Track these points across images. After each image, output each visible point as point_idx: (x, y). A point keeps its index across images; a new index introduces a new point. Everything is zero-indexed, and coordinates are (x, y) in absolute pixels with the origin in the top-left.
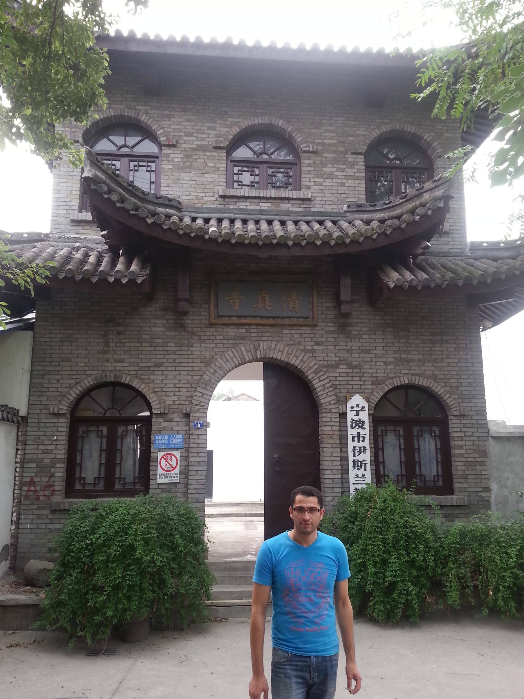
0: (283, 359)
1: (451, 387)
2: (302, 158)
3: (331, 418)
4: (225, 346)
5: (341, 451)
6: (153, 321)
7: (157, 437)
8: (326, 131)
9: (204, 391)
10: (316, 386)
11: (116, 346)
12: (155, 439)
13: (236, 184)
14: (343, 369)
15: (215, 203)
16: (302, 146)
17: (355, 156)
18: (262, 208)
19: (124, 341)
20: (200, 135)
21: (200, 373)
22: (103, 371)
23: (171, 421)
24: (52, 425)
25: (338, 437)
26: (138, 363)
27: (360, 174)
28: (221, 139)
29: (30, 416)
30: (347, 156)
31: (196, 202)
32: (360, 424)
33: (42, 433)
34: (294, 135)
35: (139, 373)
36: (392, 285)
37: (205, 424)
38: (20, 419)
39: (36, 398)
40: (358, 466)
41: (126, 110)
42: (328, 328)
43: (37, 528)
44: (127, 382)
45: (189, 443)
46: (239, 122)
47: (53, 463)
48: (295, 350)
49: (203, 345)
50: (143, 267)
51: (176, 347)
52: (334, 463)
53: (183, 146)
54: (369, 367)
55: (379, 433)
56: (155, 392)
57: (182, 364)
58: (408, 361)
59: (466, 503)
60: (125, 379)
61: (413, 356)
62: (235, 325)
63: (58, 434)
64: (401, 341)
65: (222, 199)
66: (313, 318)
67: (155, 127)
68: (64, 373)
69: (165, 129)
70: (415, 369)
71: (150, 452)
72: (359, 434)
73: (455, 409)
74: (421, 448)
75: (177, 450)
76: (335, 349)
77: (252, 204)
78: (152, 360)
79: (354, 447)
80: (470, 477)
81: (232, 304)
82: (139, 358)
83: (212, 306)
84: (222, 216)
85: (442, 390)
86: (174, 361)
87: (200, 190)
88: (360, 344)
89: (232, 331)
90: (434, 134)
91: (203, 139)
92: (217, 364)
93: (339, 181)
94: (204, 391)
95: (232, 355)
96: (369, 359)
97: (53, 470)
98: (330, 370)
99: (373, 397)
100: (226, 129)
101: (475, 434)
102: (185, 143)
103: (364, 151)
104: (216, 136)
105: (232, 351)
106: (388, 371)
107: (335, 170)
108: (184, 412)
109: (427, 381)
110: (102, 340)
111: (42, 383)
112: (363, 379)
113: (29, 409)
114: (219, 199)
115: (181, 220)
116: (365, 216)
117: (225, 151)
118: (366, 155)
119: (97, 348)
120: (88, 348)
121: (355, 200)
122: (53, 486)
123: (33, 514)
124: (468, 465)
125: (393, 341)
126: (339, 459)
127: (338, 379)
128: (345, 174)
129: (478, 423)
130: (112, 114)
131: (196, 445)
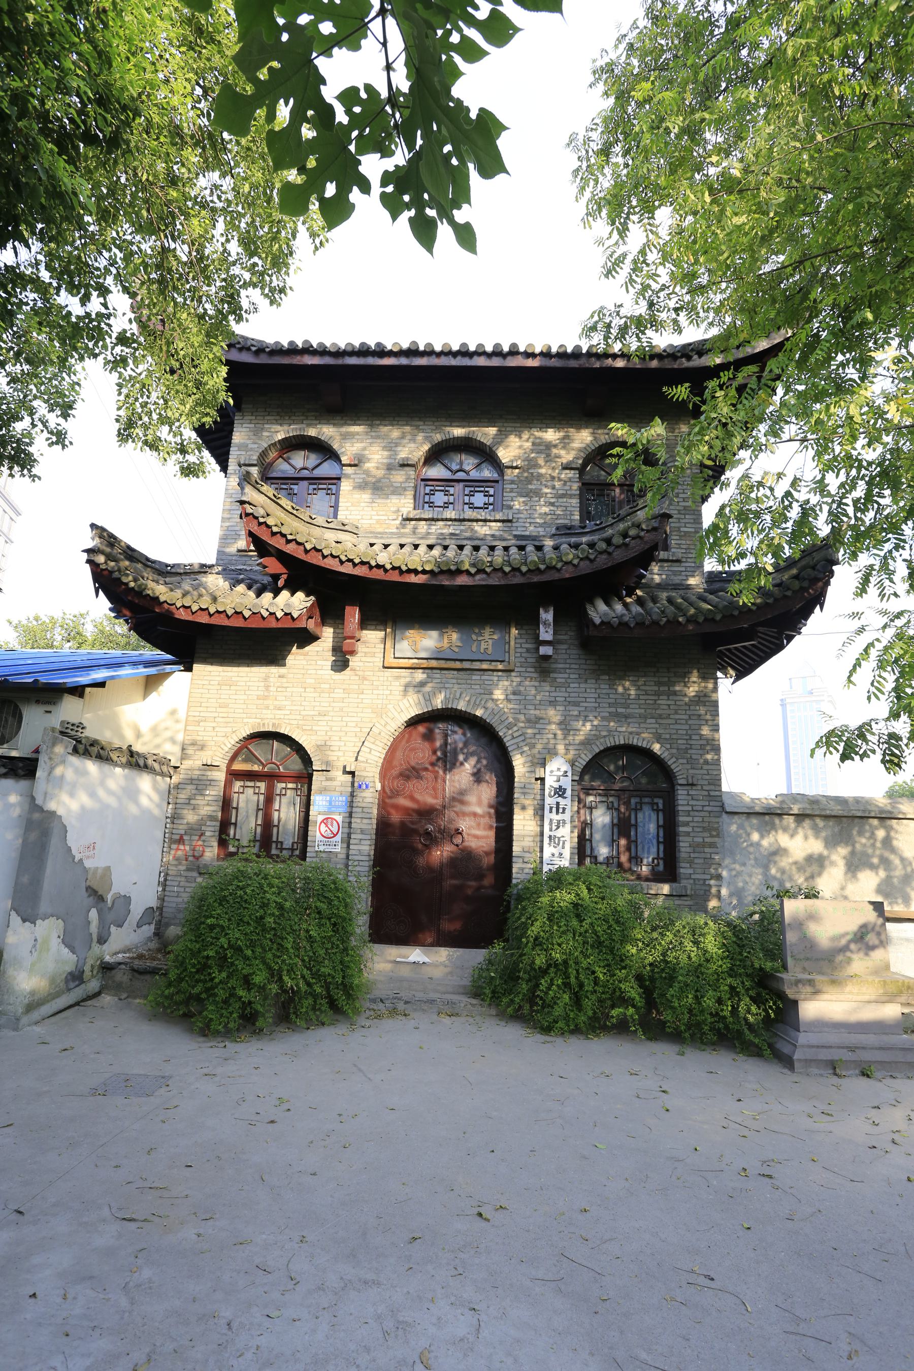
13: (426, 506)
36: (597, 621)
72: (558, 804)
74: (640, 824)
80: (696, 861)
86: (341, 710)
92: (390, 714)
101: (706, 808)
116: (573, 540)
118: (581, 470)
121: (566, 521)
124: (695, 847)
129: (709, 795)
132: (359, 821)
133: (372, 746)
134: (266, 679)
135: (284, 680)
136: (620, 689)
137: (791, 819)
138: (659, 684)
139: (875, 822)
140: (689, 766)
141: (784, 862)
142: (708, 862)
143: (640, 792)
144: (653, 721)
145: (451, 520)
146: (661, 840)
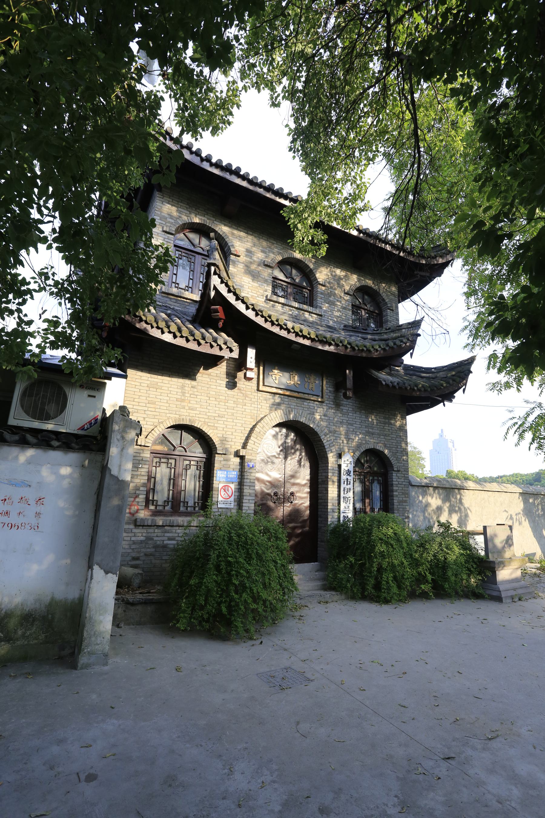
19: (196, 393)
22: (180, 415)
35: (207, 420)
68: (150, 413)
110: (180, 391)
119: (176, 396)
132: (248, 488)
133: (255, 440)
134: (183, 387)
135: (195, 390)
136: (370, 420)
137: (431, 489)
138: (385, 418)
139: (457, 491)
141: (430, 510)
142: (405, 510)
143: (373, 474)
145: (295, 308)
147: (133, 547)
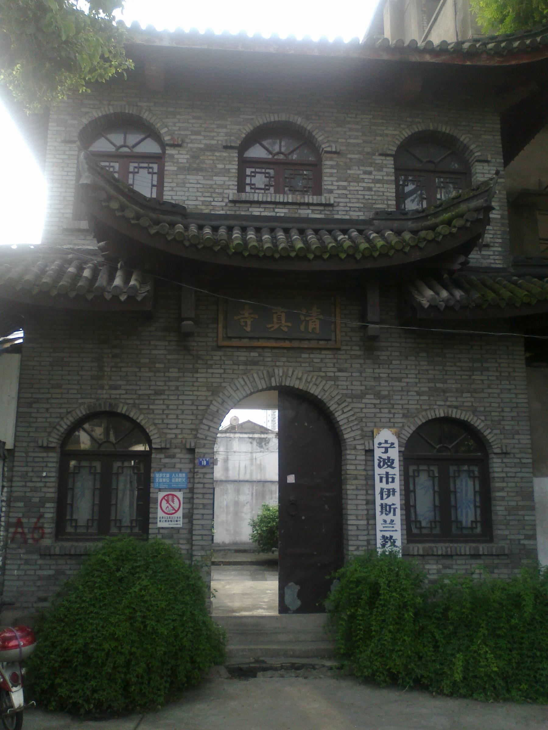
0: (301, 388)
1: (492, 421)
2: (324, 159)
3: (356, 455)
4: (235, 372)
5: (367, 494)
6: (152, 343)
7: (157, 475)
8: (350, 130)
9: (211, 424)
10: (338, 419)
11: (111, 371)
12: (154, 478)
14: (370, 399)
15: (225, 208)
16: (323, 146)
17: (383, 158)
18: (278, 215)
19: (121, 365)
20: (208, 134)
21: (206, 403)
22: (98, 399)
23: (173, 456)
24: (40, 460)
25: (363, 478)
26: (136, 390)
27: (389, 178)
28: (232, 138)
29: (16, 449)
30: (374, 157)
31: (203, 207)
32: (389, 462)
33: (30, 469)
34: (314, 133)
35: (137, 401)
37: (211, 461)
38: (6, 453)
39: (23, 429)
40: (386, 510)
41: (127, 107)
42: (353, 353)
43: (25, 575)
44: (123, 412)
45: (194, 483)
46: (253, 119)
47: (43, 501)
48: (315, 377)
49: (210, 371)
50: (143, 282)
51: (179, 372)
52: (360, 507)
53: (190, 145)
54: (399, 397)
55: (411, 473)
56: (155, 424)
57: (186, 393)
58: (445, 391)
59: (506, 552)
60: (122, 409)
61: (449, 386)
62: (246, 347)
63: (48, 469)
64: (437, 368)
65: (233, 205)
66: (336, 341)
67: (159, 125)
68: (54, 401)
69: (170, 128)
70: (452, 400)
71: (149, 492)
72: (387, 474)
73: (496, 446)
74: (458, 490)
75: (180, 490)
76: (361, 376)
77: (267, 210)
78: (152, 388)
79: (382, 490)
81: (243, 324)
82: (137, 385)
83: (220, 325)
84: (231, 223)
85: (482, 425)
86: (177, 388)
87: (207, 194)
88: (389, 371)
89: (242, 356)
90: (471, 136)
91: (212, 138)
92: (226, 393)
93: (365, 185)
94: (211, 424)
95: (243, 383)
96: (400, 389)
97: (42, 510)
98: (355, 400)
99: (404, 432)
100: (238, 127)
101: (518, 475)
102: (191, 142)
103: (394, 153)
104: (227, 134)
105: (243, 378)
106: (421, 403)
107: (361, 172)
108: (188, 447)
109: (466, 415)
111: (30, 413)
112: (393, 411)
113: (15, 441)
114: (230, 205)
115: (186, 228)
117: (237, 151)
118: (396, 157)
120: (81, 373)
122: (42, 528)
123: (21, 559)
125: (427, 368)
126: (365, 502)
127: (364, 410)
128: (372, 177)
130: (112, 111)
131: (201, 486)
132: (200, 496)
140: (502, 436)
144: (469, 395)
146: (478, 504)
147: (39, 583)
